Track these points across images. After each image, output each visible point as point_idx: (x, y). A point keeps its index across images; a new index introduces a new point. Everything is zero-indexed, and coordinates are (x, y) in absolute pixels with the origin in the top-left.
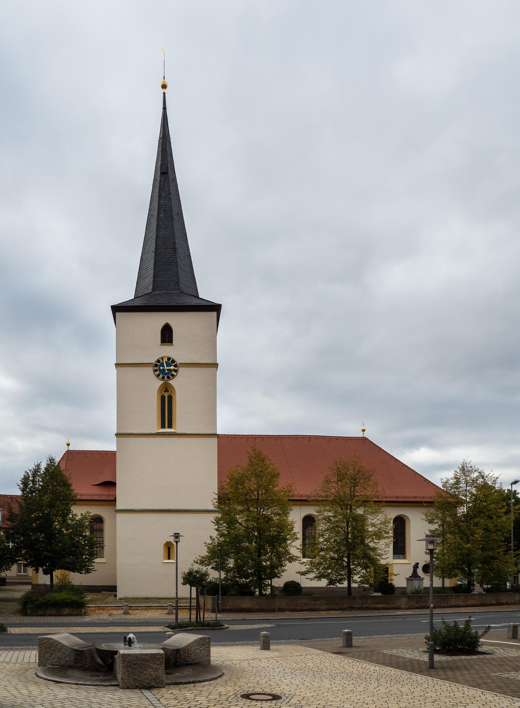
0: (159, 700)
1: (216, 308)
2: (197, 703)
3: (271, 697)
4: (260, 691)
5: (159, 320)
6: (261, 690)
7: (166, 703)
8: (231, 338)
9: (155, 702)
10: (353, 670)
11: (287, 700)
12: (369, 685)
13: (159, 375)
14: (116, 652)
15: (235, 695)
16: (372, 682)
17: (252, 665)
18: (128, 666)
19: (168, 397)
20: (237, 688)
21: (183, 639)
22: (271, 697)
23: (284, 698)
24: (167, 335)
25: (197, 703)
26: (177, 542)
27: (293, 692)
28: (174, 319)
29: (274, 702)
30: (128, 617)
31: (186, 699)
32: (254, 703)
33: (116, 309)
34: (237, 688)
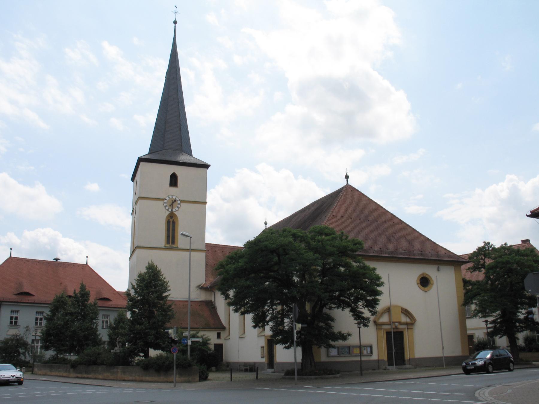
24: (174, 180)
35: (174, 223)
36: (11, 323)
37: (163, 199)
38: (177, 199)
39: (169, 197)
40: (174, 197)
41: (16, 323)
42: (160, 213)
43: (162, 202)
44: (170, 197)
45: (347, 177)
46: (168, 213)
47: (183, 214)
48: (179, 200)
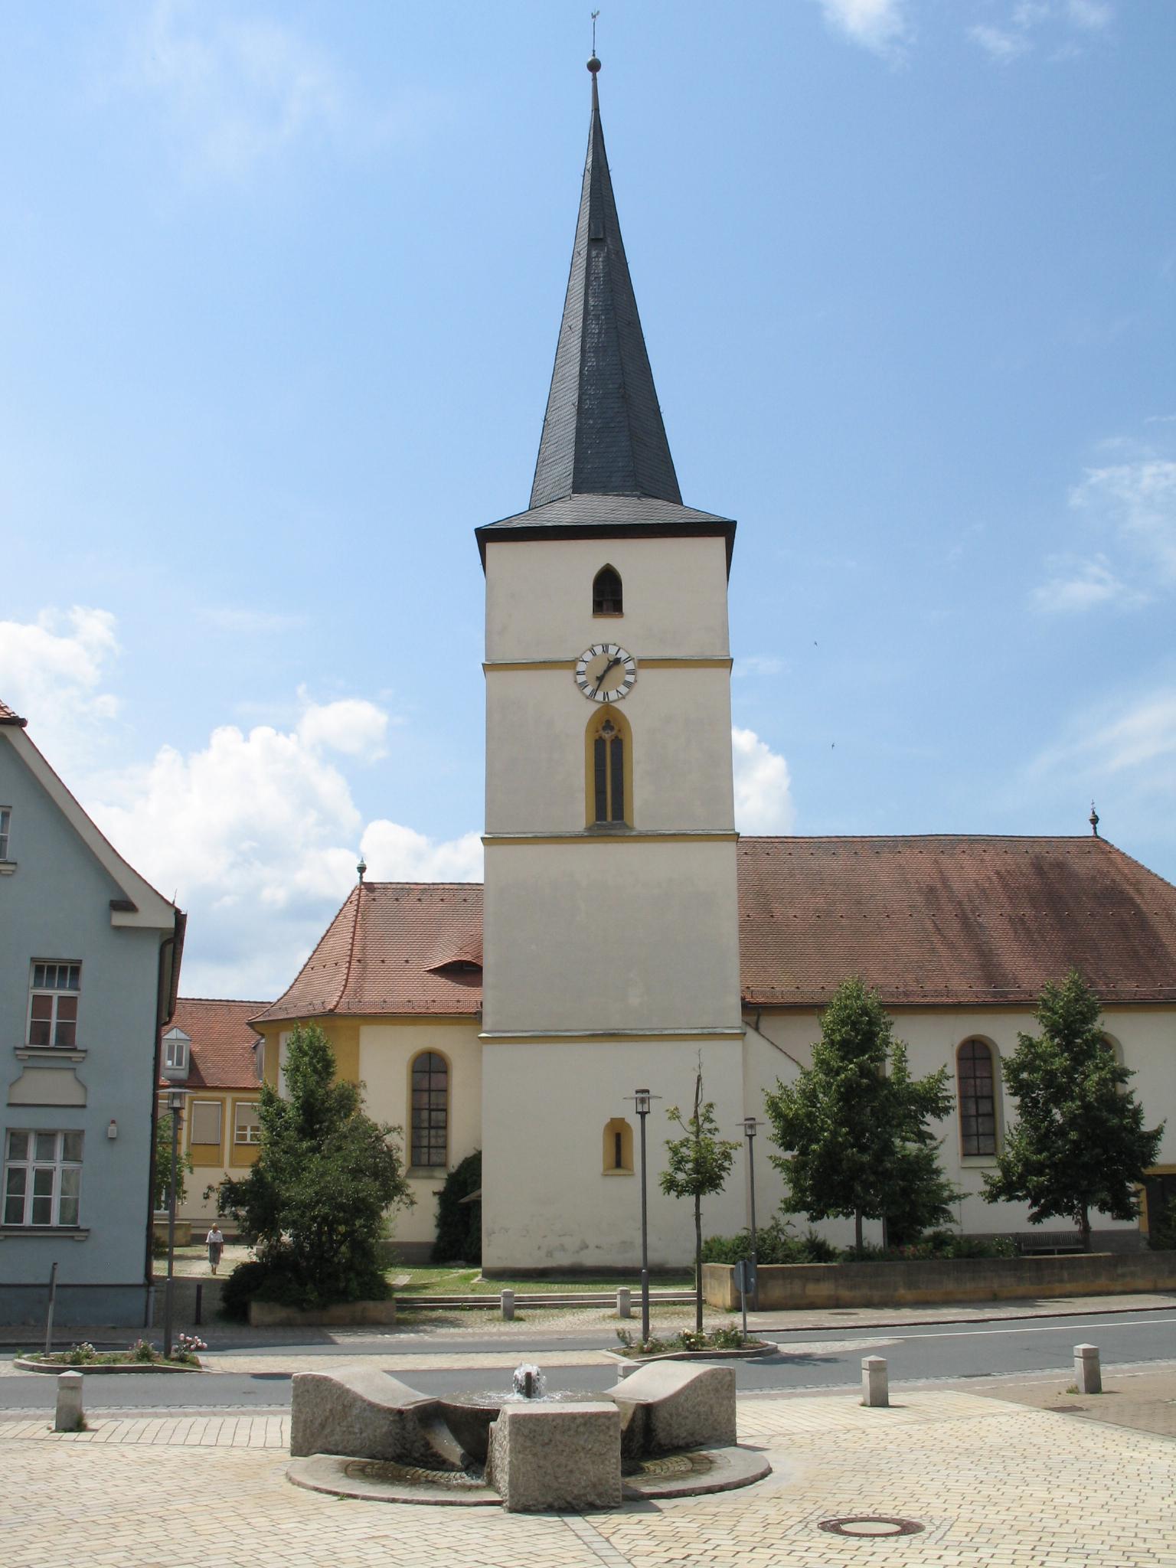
0: (607, 1540)
1: (725, 530)
2: (706, 1546)
3: (897, 1528)
4: (868, 1512)
5: (589, 558)
6: (871, 1510)
7: (628, 1547)
8: (762, 600)
9: (599, 1545)
10: (1104, 1452)
11: (938, 1534)
12: (1148, 1490)
13: (628, 684)
14: (493, 1414)
15: (805, 1523)
16: (1155, 1483)
17: (844, 1444)
18: (525, 1448)
19: (612, 742)
20: (809, 1507)
21: (662, 1380)
22: (897, 1528)
23: (929, 1528)
24: (608, 593)
25: (706, 1546)
26: (643, 1114)
27: (952, 1513)
28: (628, 558)
29: (904, 1539)
30: (514, 1327)
31: (677, 1536)
32: (853, 1542)
33: (486, 536)
34: (809, 1507)
35: (619, 746)
36: (40, 1033)
37: (571, 664)
38: (623, 655)
39: (592, 650)
40: (612, 650)
41: (66, 1034)
42: (570, 713)
43: (568, 674)
44: (599, 650)
45: (1095, 821)
46: (592, 708)
47: (645, 707)
48: (629, 659)
